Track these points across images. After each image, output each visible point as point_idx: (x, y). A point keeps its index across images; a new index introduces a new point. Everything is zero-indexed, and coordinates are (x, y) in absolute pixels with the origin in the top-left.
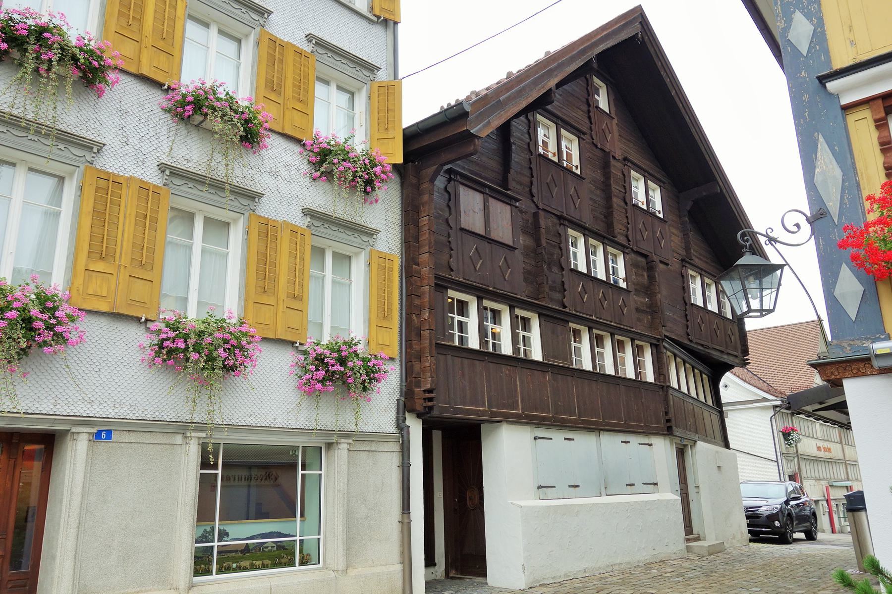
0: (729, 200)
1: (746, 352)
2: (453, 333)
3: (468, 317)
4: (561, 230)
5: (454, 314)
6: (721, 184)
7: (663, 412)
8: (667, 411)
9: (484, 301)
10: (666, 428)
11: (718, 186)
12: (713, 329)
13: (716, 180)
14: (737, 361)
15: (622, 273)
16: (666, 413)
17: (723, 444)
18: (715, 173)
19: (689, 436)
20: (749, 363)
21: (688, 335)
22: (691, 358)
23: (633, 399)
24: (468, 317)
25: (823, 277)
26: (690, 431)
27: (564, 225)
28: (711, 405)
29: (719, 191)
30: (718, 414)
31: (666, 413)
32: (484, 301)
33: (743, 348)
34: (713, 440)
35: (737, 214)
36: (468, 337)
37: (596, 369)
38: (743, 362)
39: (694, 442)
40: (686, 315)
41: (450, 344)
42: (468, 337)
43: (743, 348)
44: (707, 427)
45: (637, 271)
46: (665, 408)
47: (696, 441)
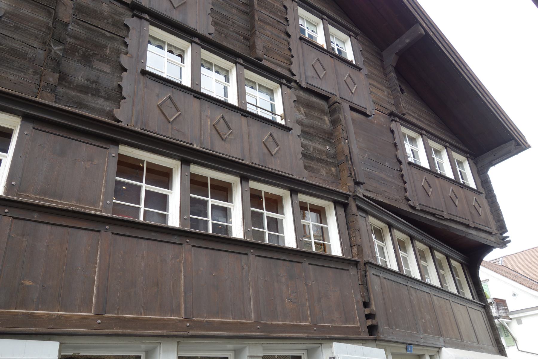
0: (440, 45)
1: (502, 228)
2: (165, 215)
3: (232, 202)
4: (393, 125)
5: (208, 197)
6: (425, 25)
7: (358, 302)
8: (367, 300)
9: (299, 194)
10: (365, 329)
11: (420, 27)
12: (449, 197)
13: (417, 21)
14: (492, 238)
15: (279, 110)
16: (366, 305)
17: (494, 349)
18: (416, 14)
19: (422, 340)
20: (509, 241)
21: (408, 200)
22: (422, 234)
23: (283, 280)
24: (232, 202)
25: (327, 27)
26: (425, 332)
27: (396, 121)
28: (471, 298)
29: (424, 33)
30: (483, 310)
31: (366, 305)
32: (299, 194)
33: (499, 224)
34: (476, 345)
35: (453, 61)
36: (231, 226)
37: (245, 238)
38: (502, 241)
39: (437, 350)
40: (402, 176)
41: (262, 243)
42: (268, 231)
43: (499, 224)
44: (462, 327)
45: (309, 112)
46: (363, 297)
47: (440, 348)
